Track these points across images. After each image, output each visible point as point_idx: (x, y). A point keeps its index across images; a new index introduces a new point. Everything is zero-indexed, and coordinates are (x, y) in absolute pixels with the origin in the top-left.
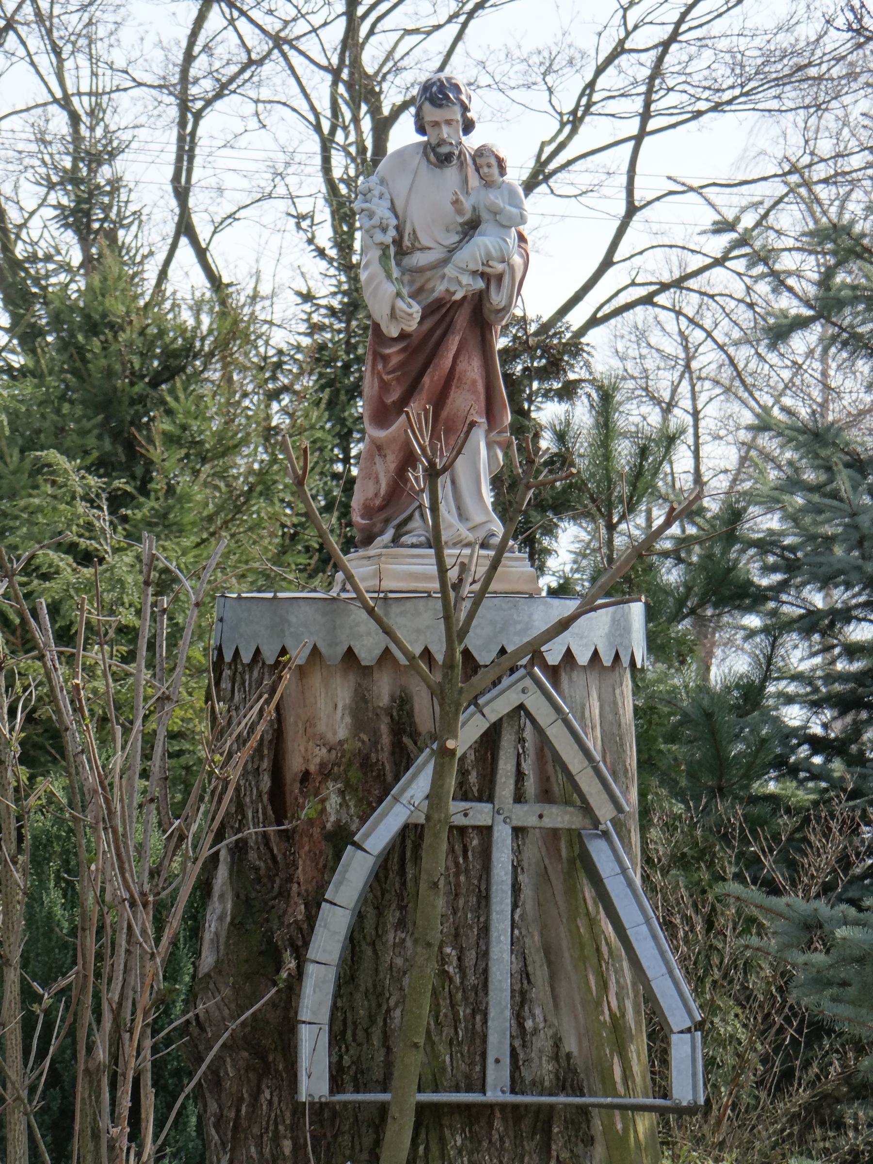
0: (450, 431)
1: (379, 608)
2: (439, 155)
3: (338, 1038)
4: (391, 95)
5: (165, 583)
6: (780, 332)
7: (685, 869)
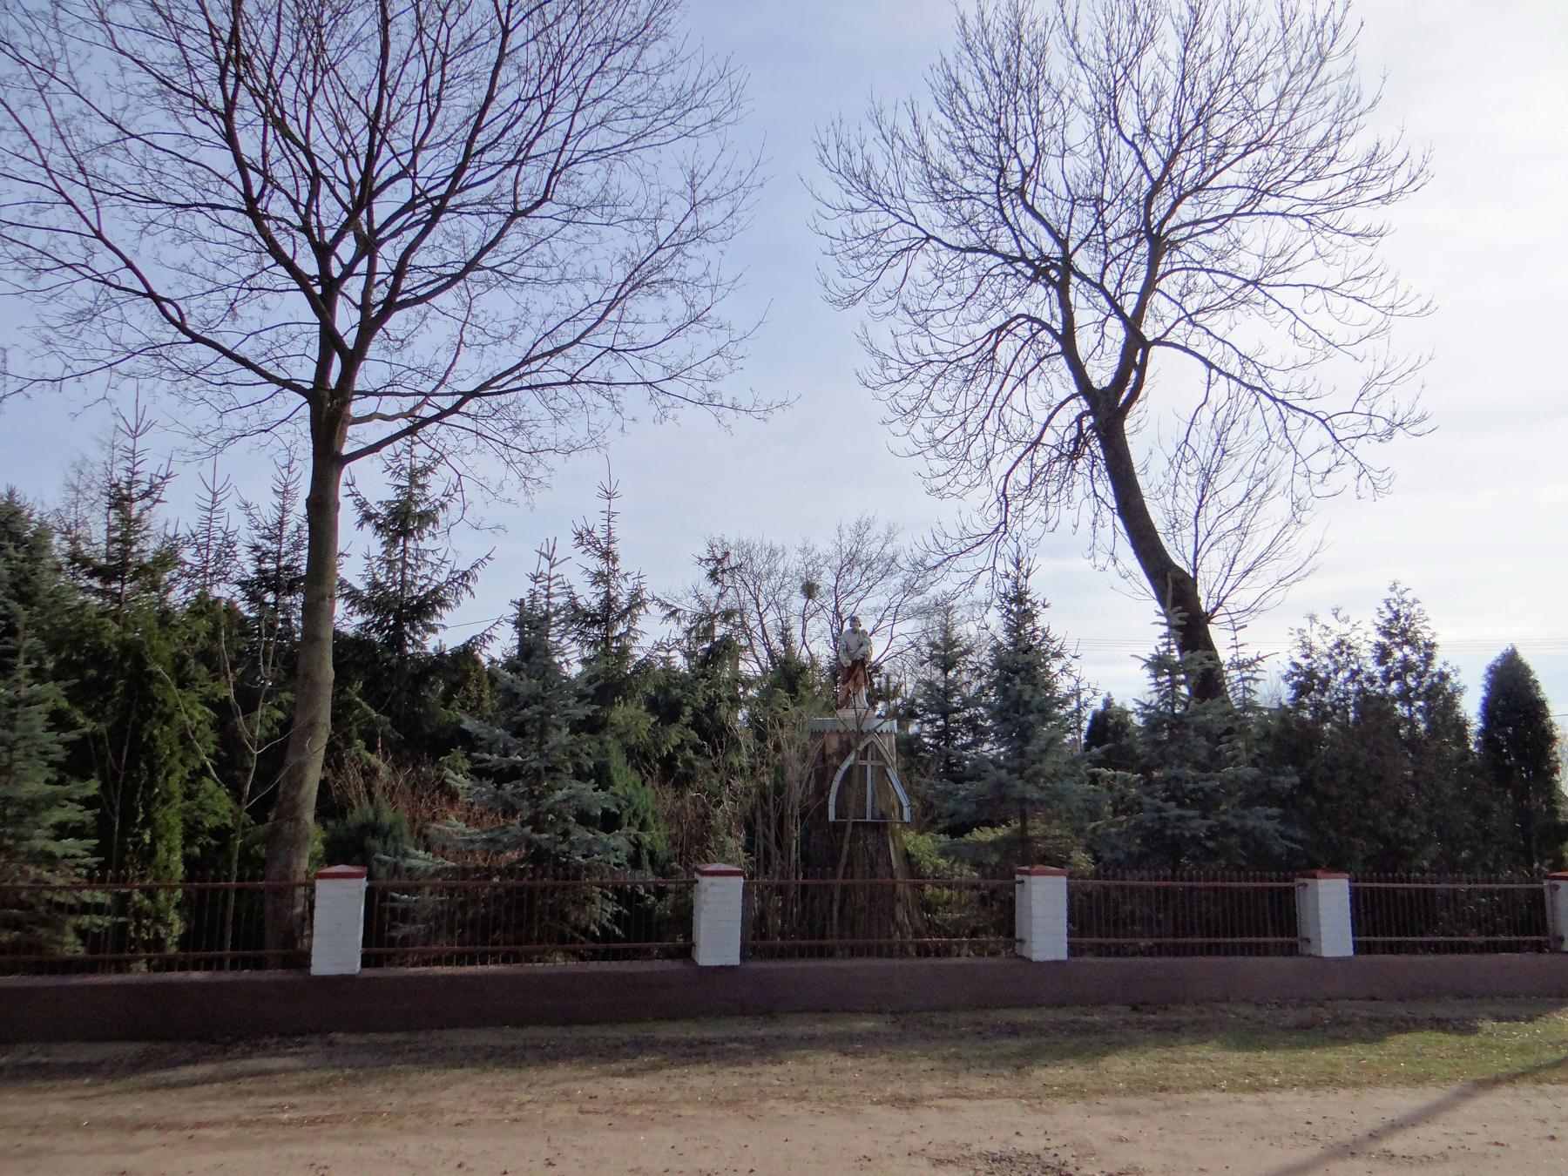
0: (858, 686)
1: (844, 722)
2: (854, 631)
3: (836, 808)
4: (844, 617)
5: (800, 715)
6: (922, 663)
7: (907, 772)
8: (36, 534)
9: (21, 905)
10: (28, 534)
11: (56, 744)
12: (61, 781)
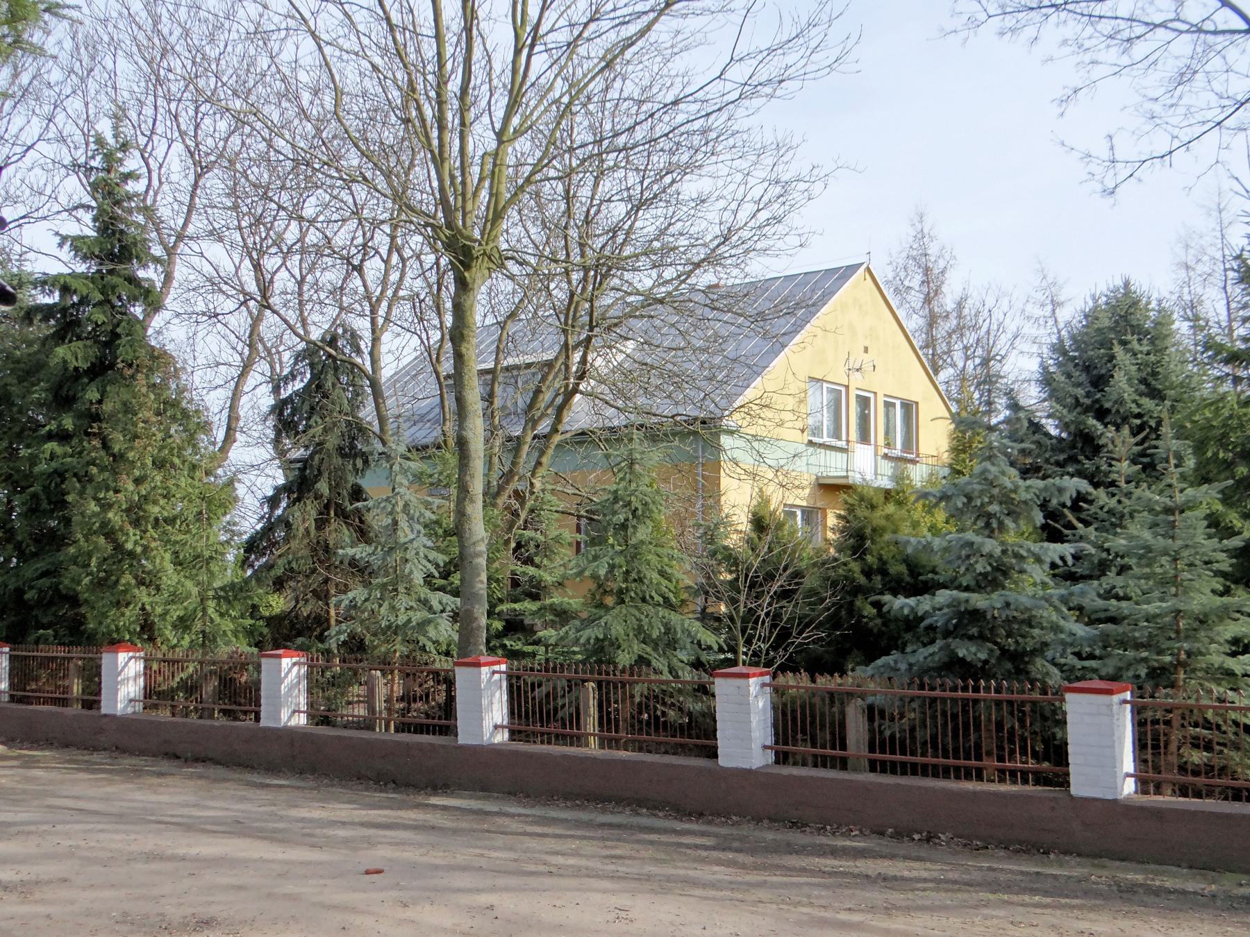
8: (1157, 324)
9: (1208, 725)
10: (1148, 325)
11: (1220, 554)
12: (1226, 592)
